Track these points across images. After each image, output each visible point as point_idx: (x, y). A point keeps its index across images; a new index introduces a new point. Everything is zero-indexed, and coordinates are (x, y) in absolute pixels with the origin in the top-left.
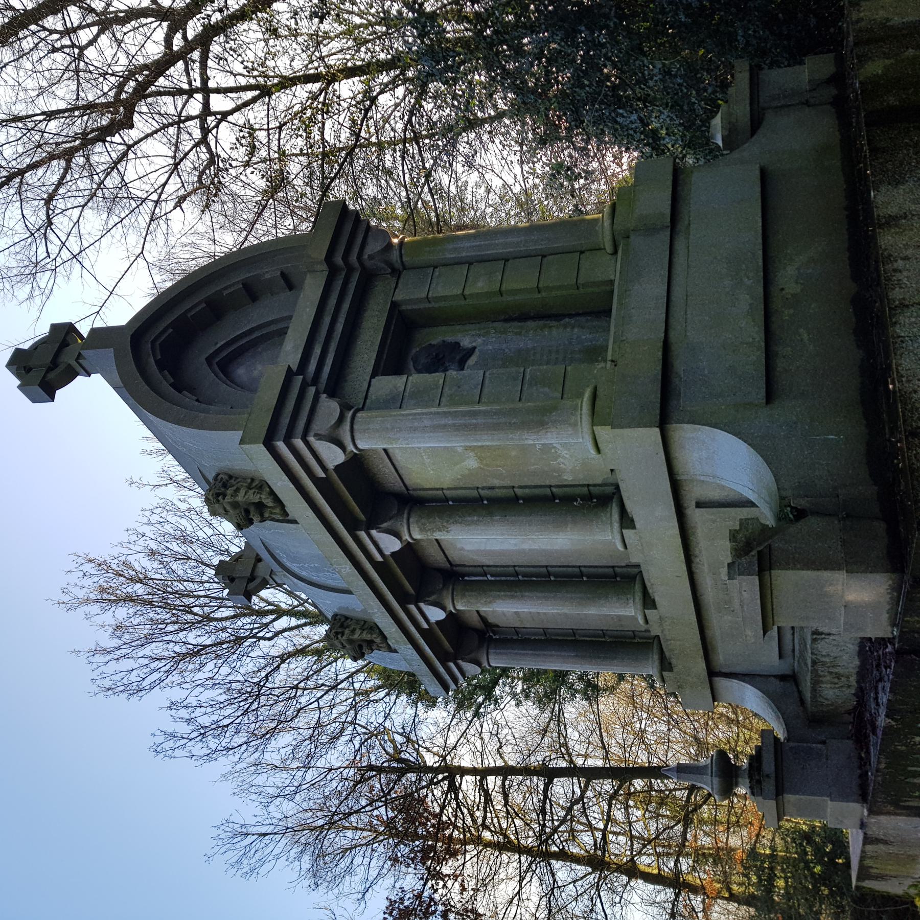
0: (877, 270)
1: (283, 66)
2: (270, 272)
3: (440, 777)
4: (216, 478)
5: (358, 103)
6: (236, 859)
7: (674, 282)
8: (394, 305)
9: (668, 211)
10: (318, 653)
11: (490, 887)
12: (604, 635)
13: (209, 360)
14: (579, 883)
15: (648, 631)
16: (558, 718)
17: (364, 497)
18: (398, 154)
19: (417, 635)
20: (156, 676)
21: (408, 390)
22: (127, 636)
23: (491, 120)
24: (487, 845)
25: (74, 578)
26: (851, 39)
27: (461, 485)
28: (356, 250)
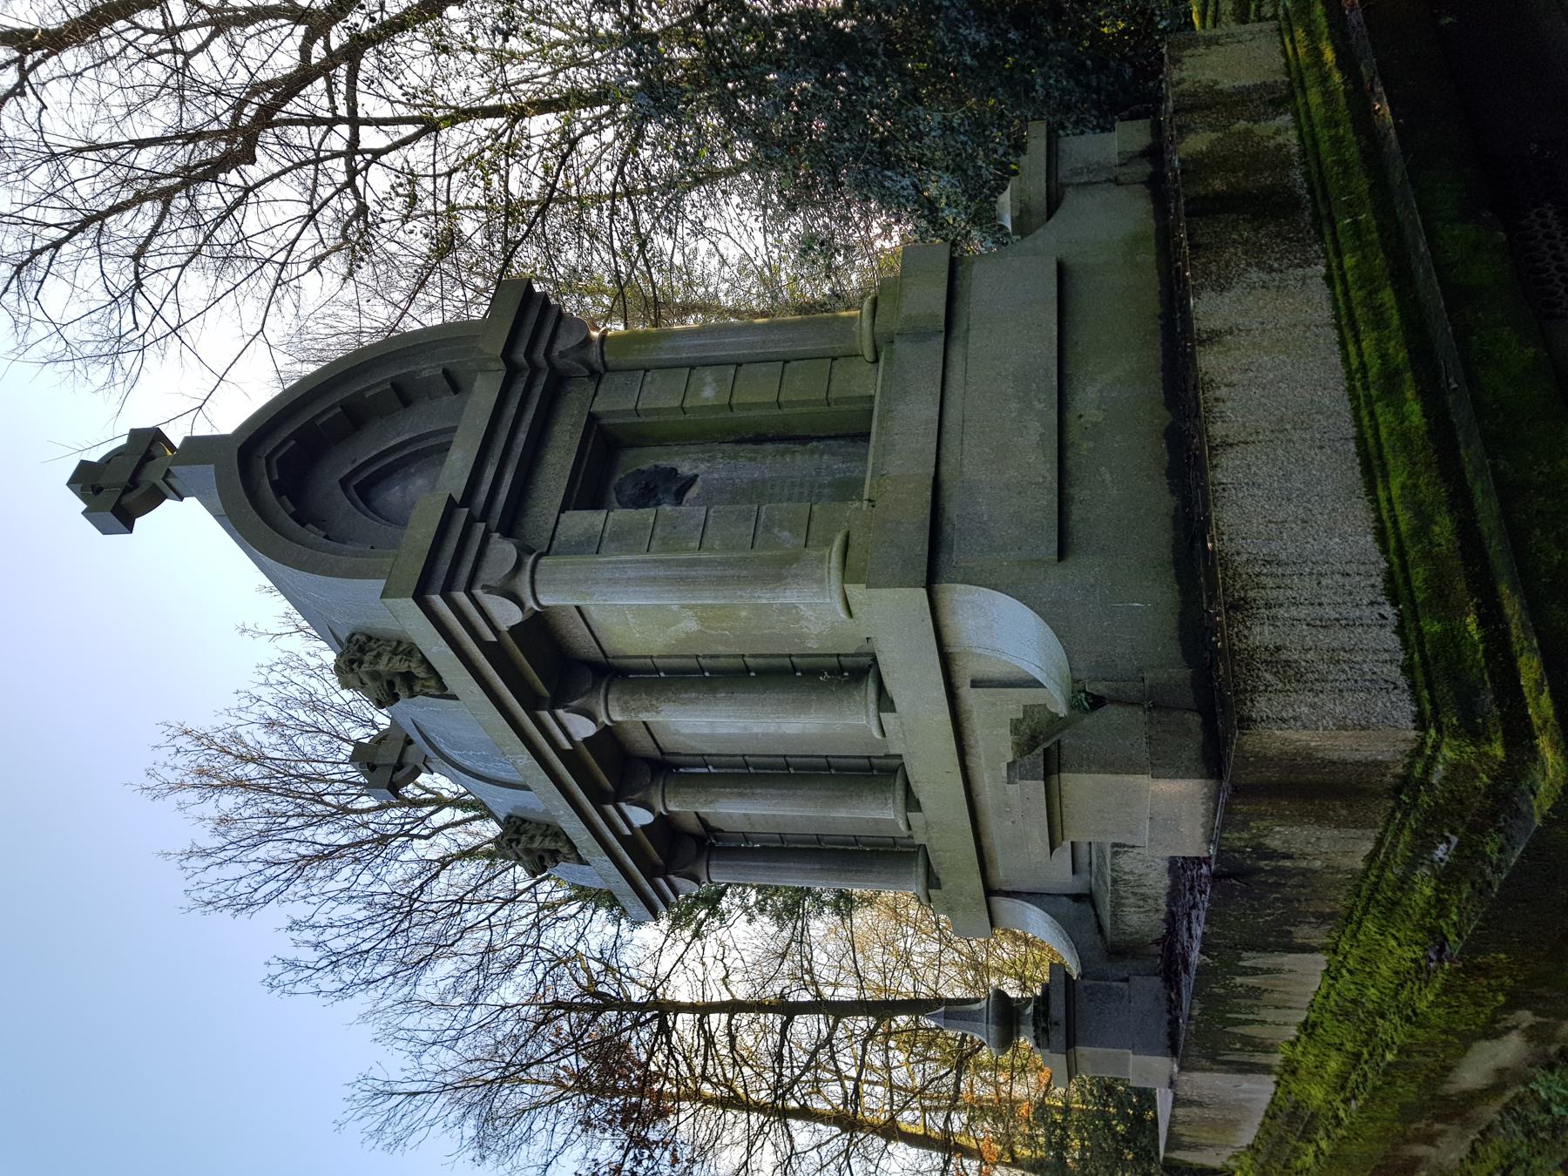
0: (1196, 397)
1: (454, 92)
2: (428, 369)
3: (648, 1015)
4: (349, 640)
5: (554, 146)
6: (376, 1126)
7: (947, 402)
8: (592, 418)
9: (942, 312)
10: (490, 855)
11: (710, 1155)
12: (857, 843)
13: (344, 483)
14: (824, 1149)
15: (910, 837)
16: (800, 939)
17: (548, 666)
18: (606, 213)
19: (616, 844)
20: (272, 886)
21: (608, 527)
22: (234, 833)
23: (728, 173)
24: (707, 1101)
25: (164, 755)
26: (1170, 104)
27: (676, 652)
28: (543, 344)
